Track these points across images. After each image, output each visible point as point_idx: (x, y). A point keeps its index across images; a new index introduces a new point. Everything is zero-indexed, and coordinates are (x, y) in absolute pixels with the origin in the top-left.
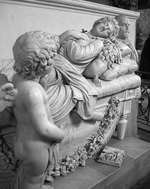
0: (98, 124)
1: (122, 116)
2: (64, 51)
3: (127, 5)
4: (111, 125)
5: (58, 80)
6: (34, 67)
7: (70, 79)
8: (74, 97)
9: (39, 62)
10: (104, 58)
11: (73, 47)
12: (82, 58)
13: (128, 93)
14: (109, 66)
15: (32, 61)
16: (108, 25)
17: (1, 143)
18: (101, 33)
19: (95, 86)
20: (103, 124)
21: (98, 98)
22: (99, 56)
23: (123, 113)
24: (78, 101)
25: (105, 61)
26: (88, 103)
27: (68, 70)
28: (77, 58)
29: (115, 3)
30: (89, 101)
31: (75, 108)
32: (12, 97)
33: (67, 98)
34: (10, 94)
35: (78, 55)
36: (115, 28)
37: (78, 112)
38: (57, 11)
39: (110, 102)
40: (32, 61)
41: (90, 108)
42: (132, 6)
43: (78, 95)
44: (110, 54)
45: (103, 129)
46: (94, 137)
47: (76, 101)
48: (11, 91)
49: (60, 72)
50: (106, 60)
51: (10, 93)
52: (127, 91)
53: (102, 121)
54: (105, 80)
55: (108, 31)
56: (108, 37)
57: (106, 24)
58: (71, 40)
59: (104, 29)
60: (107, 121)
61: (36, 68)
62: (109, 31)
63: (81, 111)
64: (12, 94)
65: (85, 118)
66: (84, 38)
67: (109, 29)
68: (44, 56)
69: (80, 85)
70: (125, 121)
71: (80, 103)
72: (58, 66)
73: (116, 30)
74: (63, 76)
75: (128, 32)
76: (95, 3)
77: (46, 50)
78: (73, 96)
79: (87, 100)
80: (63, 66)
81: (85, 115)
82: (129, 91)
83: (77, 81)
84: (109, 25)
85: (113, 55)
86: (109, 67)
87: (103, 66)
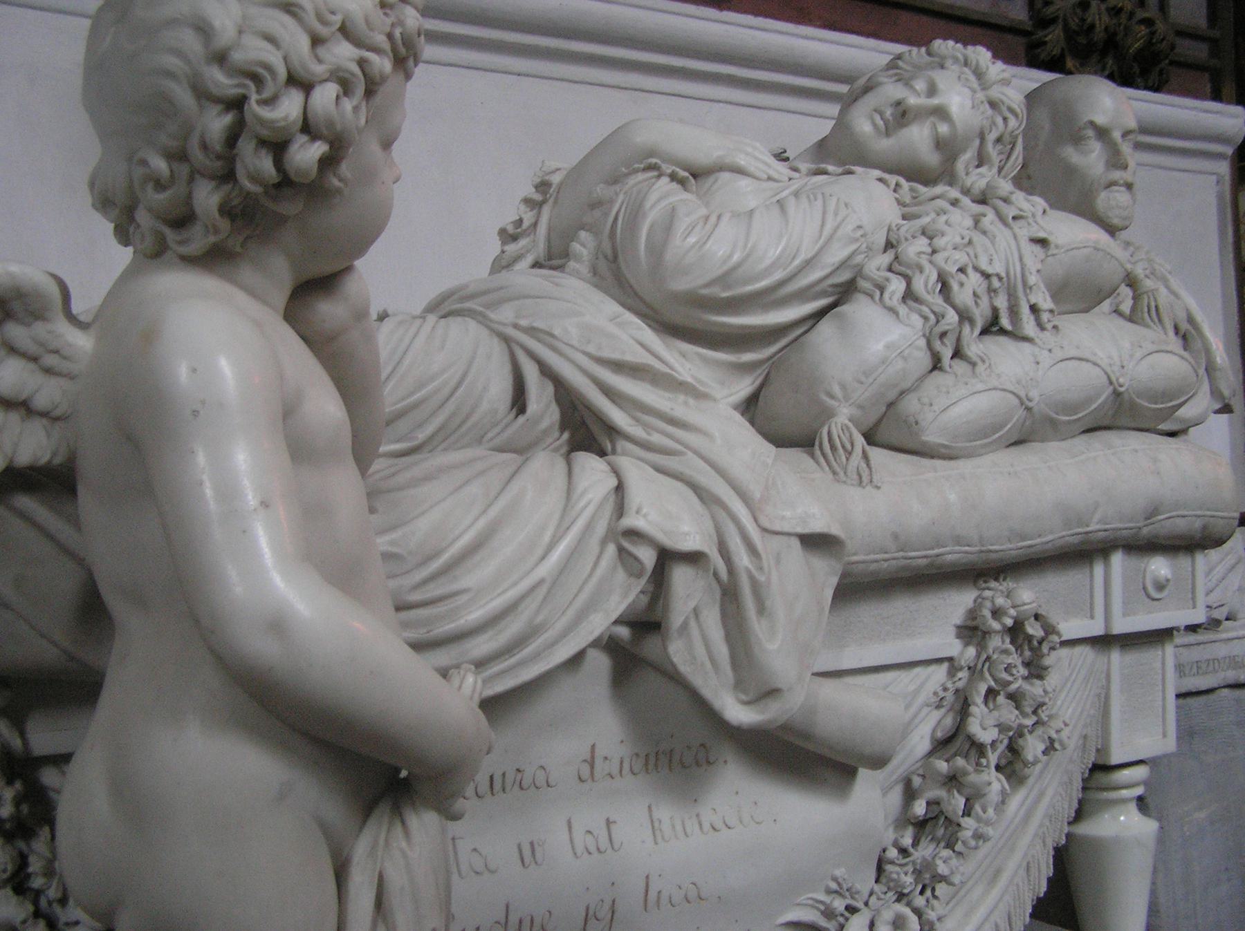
0: (871, 802)
1: (1103, 778)
4: (991, 811)
5: (521, 419)
6: (204, 146)
7: (618, 417)
8: (630, 521)
9: (237, 104)
10: (897, 286)
12: (723, 279)
14: (937, 345)
15: (184, 97)
16: (932, 91)
17: (6, 811)
18: (884, 145)
19: (820, 476)
20: (920, 808)
22: (866, 278)
23: (1103, 750)
24: (667, 557)
25: (903, 310)
28: (681, 285)
29: (1045, 43)
30: (761, 569)
31: (647, 622)
32: (54, 381)
34: (35, 359)
36: (993, 104)
37: (678, 652)
38: (617, 94)
39: (971, 631)
40: (184, 97)
43: (669, 515)
44: (939, 258)
45: (925, 851)
46: (848, 908)
47: (647, 557)
48: (39, 329)
49: (546, 371)
50: (917, 300)
51: (32, 348)
52: (1117, 559)
55: (934, 127)
56: (946, 174)
57: (920, 85)
58: (641, 176)
59: (904, 114)
60: (953, 780)
61: (218, 148)
62: (943, 129)
63: (696, 646)
64: (50, 360)
65: (738, 713)
67: (941, 113)
68: (274, 58)
69: (690, 454)
70: (1123, 825)
71: (681, 576)
72: (532, 331)
73: (999, 120)
74: (567, 398)
75: (1129, 186)
76: (872, 42)
77: (293, 15)
78: (620, 510)
79: (743, 560)
80: (568, 329)
81: (739, 685)
82: (1135, 562)
83: (670, 429)
84: (941, 85)
85: (970, 270)
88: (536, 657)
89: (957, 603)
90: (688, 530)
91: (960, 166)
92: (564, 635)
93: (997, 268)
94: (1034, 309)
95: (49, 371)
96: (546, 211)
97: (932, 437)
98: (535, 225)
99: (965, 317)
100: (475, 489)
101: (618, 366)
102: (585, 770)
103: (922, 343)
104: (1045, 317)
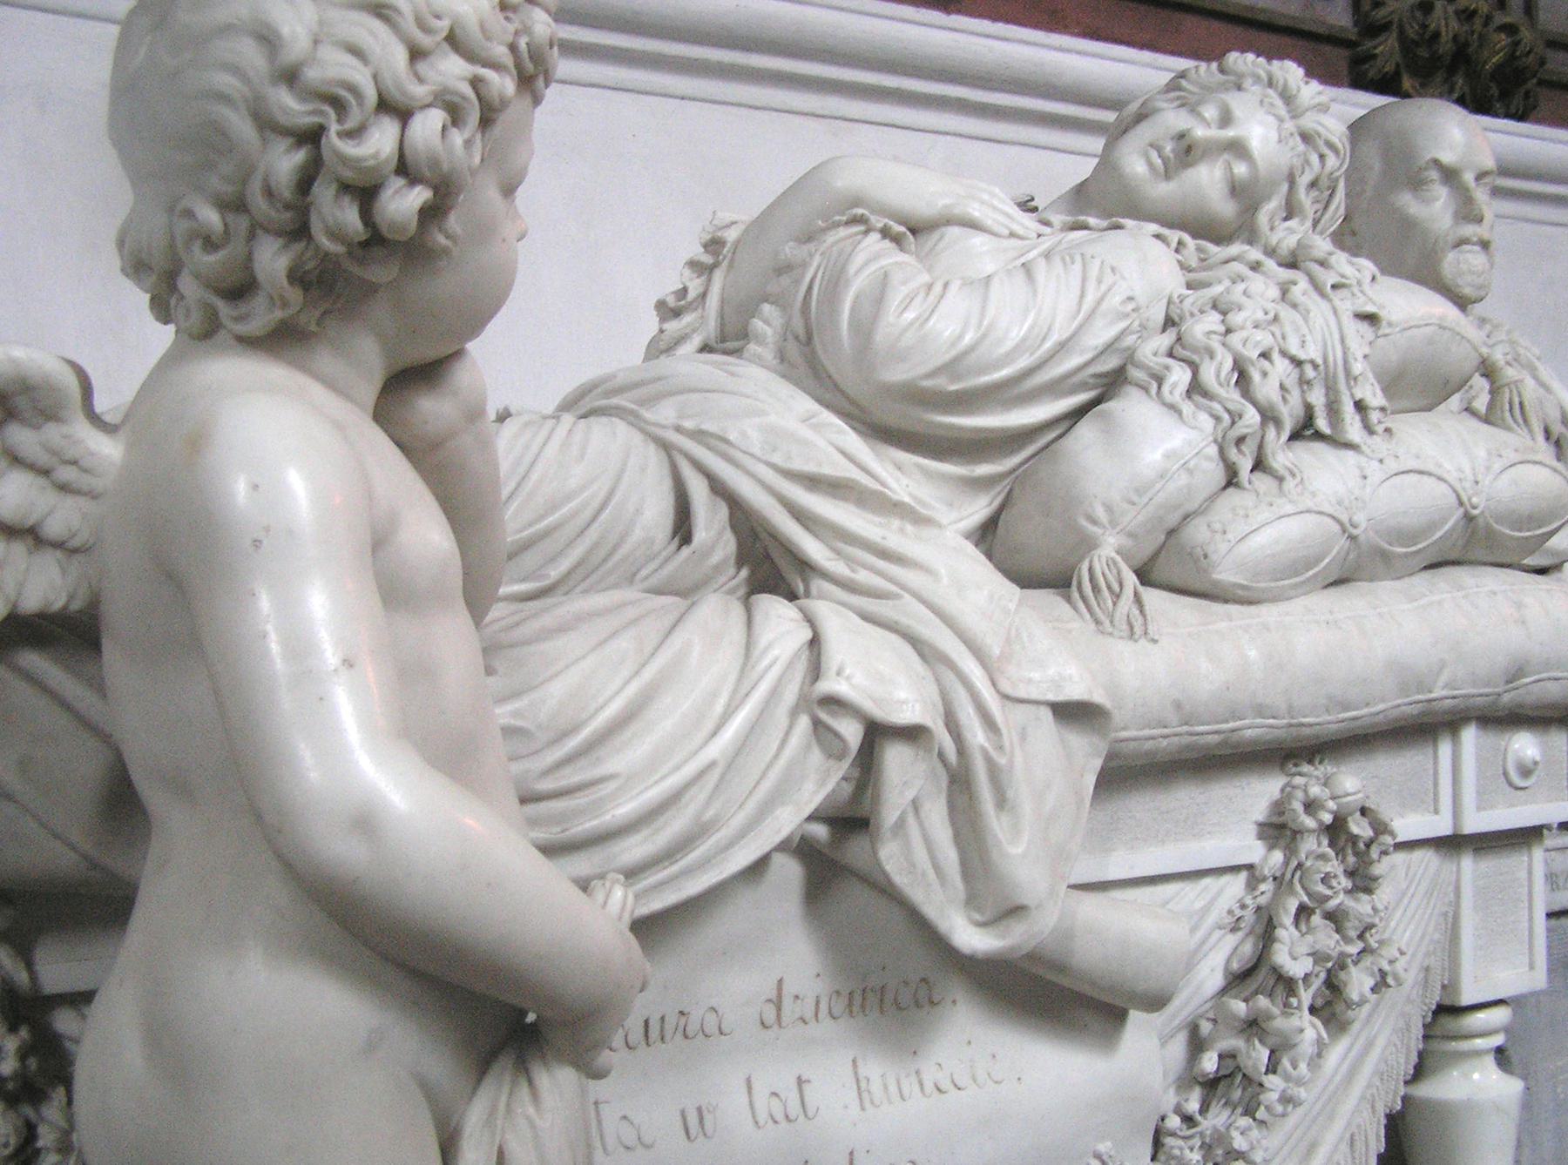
0: (1145, 1054)
1: (1450, 1024)
2: (786, 333)
3: (1493, 77)
4: (1303, 1066)
5: (686, 551)
6: (269, 193)
7: (813, 548)
9: (312, 137)
10: (1179, 376)
11: (867, 272)
12: (951, 368)
13: (1480, 760)
14: (1233, 454)
15: (242, 128)
16: (1226, 119)
18: (1162, 191)
20: (1209, 1063)
21: (1139, 770)
23: (1450, 987)
24: (876, 733)
25: (1187, 408)
26: (994, 771)
27: (798, 465)
28: (897, 374)
29: (1374, 57)
30: (1000, 748)
31: (851, 819)
32: (69, 501)
33: (761, 678)
34: (45, 472)
35: (909, 339)
36: (1306, 137)
37: (889, 857)
39: (1277, 830)
40: (242, 128)
41: (1016, 830)
42: (1543, 93)
44: (1235, 339)
47: (852, 732)
48: (52, 432)
49: (719, 488)
50: (1206, 394)
52: (1469, 735)
53: (1206, 1027)
54: (1197, 585)
56: (1245, 228)
57: (1210, 112)
58: (843, 232)
59: (1189, 149)
60: (1253, 1026)
62: (1241, 169)
63: (915, 849)
64: (66, 474)
66: (975, 211)
67: (1237, 148)
68: (361, 77)
71: (896, 760)
72: (699, 435)
73: (1314, 159)
74: (745, 522)
78: (816, 671)
79: (977, 736)
80: (747, 433)
81: (972, 901)
82: (1492, 739)
83: (881, 564)
85: (1276, 356)
86: (1240, 466)
87: (1167, 456)
88: (688, 872)
89: (1259, 793)
90: (904, 697)
91: (1263, 218)
92: (742, 834)
93: (1312, 352)
94: (1360, 406)
95: (64, 488)
96: (718, 276)
97: (1225, 574)
98: (704, 295)
99: (1269, 416)
100: (624, 643)
101: (813, 482)
102: (770, 1015)
103: (1213, 450)
104: (1374, 416)
